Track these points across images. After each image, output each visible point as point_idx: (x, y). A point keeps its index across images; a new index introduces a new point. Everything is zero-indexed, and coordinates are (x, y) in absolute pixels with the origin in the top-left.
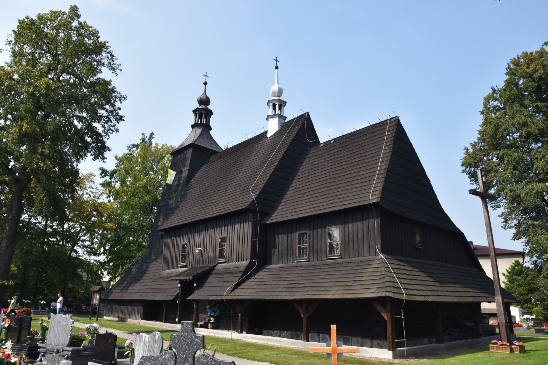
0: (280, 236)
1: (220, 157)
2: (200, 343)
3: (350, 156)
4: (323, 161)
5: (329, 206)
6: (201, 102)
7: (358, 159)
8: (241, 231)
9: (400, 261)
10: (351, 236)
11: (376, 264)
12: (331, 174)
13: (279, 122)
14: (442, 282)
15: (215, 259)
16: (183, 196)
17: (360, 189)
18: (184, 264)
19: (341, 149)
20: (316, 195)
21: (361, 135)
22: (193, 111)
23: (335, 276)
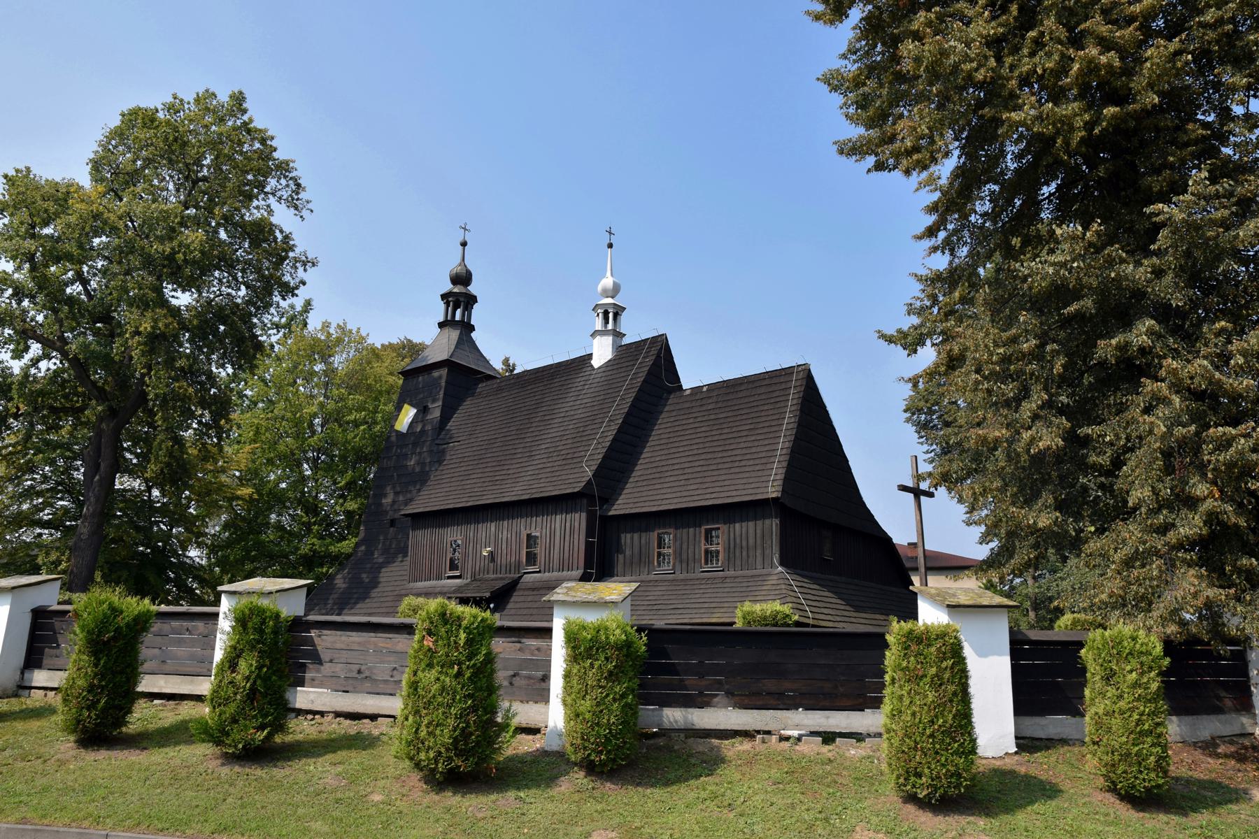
0: (629, 536)
1: (500, 389)
3: (735, 419)
4: (691, 421)
5: (708, 496)
6: (456, 280)
7: (748, 427)
8: (568, 524)
9: (803, 576)
10: (738, 541)
11: (773, 580)
12: (707, 445)
13: (614, 342)
14: (858, 609)
15: (518, 565)
16: (439, 457)
17: (753, 474)
19: (719, 405)
20: (686, 477)
21: (750, 386)
23: (718, 595)
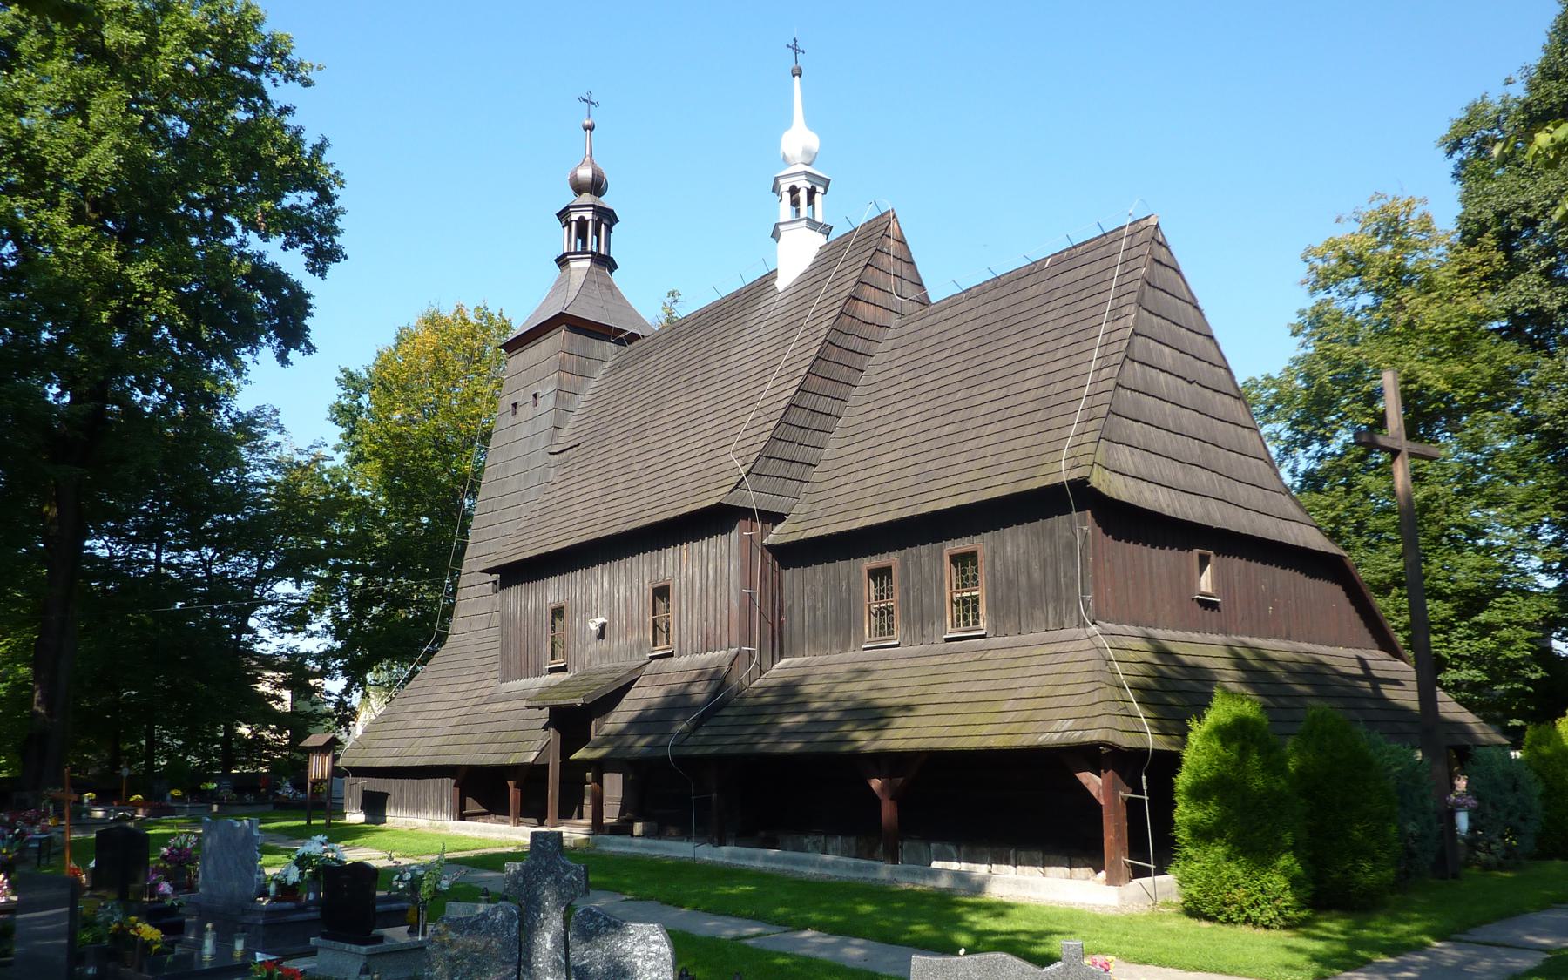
2: (577, 882)
22: (558, 215)
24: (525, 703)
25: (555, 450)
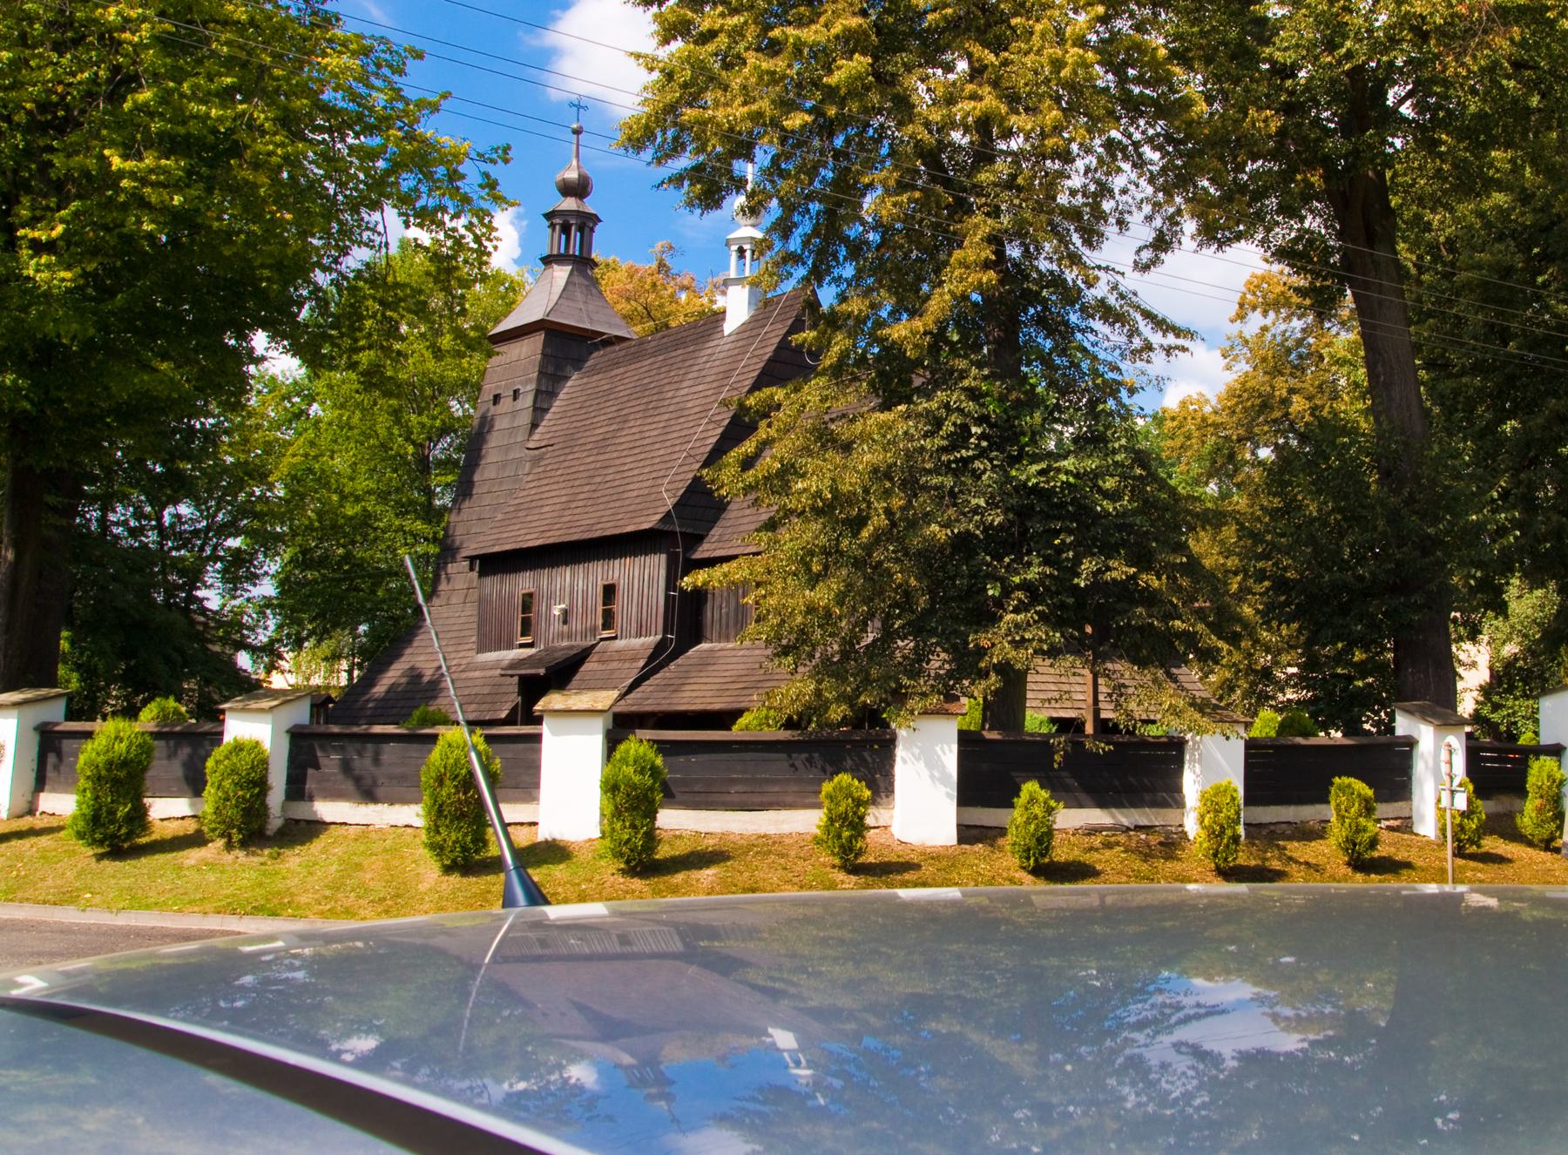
18: (528, 640)
24: (499, 672)
25: (531, 445)
